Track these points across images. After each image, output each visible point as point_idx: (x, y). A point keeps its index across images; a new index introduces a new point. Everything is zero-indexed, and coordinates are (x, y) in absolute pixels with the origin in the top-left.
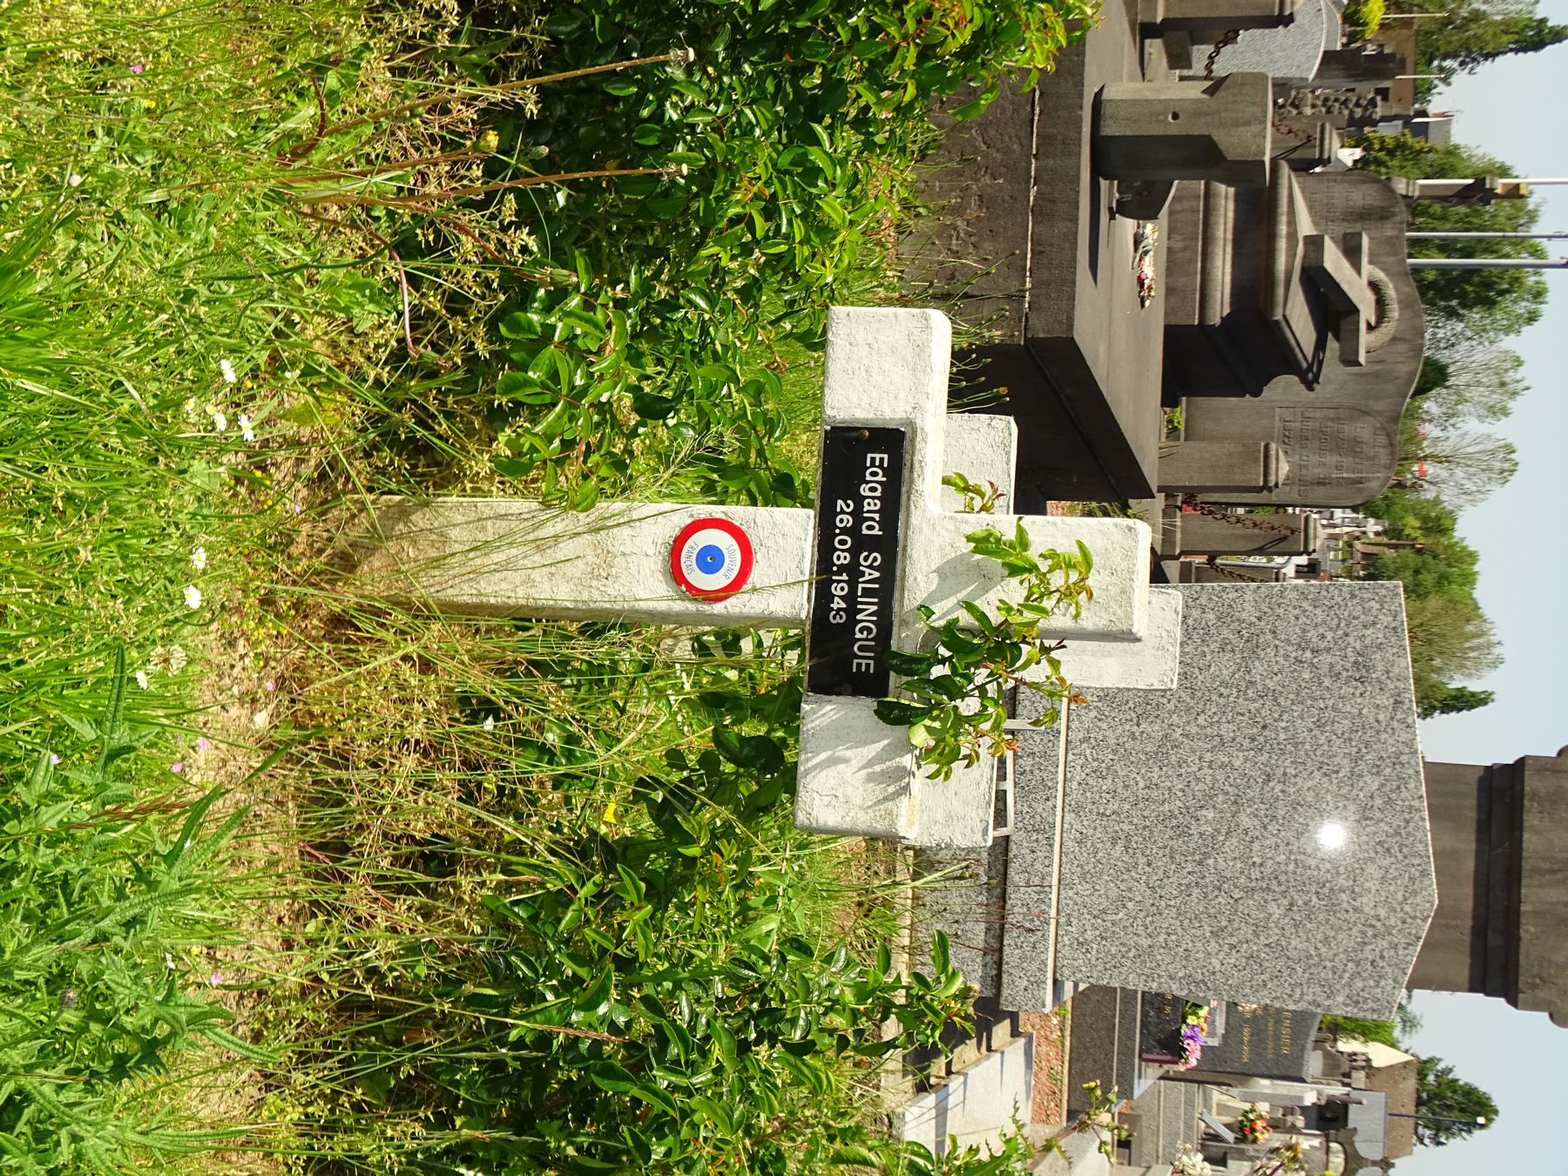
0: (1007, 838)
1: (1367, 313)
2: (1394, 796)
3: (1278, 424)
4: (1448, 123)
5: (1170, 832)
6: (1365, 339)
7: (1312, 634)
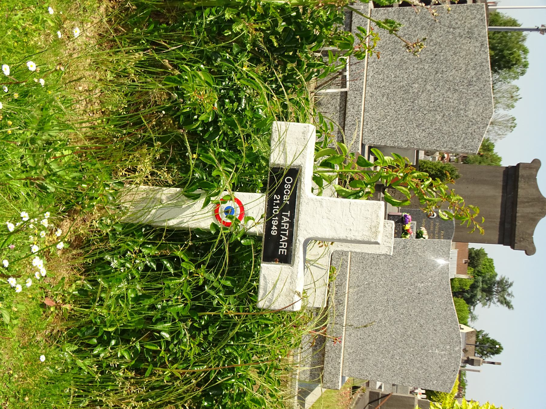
0: (346, 92)
2: (480, 77)
5: (402, 92)
7: (453, 23)
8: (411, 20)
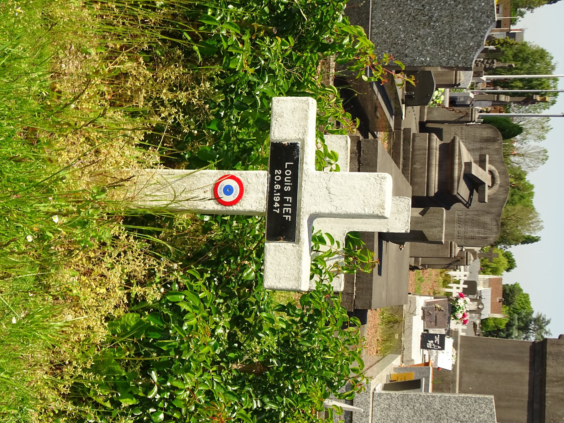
1: (488, 182)
3: (456, 216)
4: (523, 33)
6: (488, 192)
7: (461, 415)
8: (416, 408)
